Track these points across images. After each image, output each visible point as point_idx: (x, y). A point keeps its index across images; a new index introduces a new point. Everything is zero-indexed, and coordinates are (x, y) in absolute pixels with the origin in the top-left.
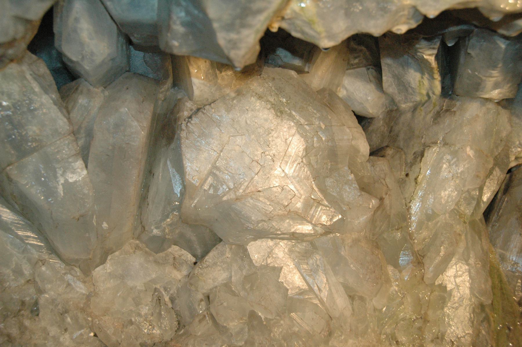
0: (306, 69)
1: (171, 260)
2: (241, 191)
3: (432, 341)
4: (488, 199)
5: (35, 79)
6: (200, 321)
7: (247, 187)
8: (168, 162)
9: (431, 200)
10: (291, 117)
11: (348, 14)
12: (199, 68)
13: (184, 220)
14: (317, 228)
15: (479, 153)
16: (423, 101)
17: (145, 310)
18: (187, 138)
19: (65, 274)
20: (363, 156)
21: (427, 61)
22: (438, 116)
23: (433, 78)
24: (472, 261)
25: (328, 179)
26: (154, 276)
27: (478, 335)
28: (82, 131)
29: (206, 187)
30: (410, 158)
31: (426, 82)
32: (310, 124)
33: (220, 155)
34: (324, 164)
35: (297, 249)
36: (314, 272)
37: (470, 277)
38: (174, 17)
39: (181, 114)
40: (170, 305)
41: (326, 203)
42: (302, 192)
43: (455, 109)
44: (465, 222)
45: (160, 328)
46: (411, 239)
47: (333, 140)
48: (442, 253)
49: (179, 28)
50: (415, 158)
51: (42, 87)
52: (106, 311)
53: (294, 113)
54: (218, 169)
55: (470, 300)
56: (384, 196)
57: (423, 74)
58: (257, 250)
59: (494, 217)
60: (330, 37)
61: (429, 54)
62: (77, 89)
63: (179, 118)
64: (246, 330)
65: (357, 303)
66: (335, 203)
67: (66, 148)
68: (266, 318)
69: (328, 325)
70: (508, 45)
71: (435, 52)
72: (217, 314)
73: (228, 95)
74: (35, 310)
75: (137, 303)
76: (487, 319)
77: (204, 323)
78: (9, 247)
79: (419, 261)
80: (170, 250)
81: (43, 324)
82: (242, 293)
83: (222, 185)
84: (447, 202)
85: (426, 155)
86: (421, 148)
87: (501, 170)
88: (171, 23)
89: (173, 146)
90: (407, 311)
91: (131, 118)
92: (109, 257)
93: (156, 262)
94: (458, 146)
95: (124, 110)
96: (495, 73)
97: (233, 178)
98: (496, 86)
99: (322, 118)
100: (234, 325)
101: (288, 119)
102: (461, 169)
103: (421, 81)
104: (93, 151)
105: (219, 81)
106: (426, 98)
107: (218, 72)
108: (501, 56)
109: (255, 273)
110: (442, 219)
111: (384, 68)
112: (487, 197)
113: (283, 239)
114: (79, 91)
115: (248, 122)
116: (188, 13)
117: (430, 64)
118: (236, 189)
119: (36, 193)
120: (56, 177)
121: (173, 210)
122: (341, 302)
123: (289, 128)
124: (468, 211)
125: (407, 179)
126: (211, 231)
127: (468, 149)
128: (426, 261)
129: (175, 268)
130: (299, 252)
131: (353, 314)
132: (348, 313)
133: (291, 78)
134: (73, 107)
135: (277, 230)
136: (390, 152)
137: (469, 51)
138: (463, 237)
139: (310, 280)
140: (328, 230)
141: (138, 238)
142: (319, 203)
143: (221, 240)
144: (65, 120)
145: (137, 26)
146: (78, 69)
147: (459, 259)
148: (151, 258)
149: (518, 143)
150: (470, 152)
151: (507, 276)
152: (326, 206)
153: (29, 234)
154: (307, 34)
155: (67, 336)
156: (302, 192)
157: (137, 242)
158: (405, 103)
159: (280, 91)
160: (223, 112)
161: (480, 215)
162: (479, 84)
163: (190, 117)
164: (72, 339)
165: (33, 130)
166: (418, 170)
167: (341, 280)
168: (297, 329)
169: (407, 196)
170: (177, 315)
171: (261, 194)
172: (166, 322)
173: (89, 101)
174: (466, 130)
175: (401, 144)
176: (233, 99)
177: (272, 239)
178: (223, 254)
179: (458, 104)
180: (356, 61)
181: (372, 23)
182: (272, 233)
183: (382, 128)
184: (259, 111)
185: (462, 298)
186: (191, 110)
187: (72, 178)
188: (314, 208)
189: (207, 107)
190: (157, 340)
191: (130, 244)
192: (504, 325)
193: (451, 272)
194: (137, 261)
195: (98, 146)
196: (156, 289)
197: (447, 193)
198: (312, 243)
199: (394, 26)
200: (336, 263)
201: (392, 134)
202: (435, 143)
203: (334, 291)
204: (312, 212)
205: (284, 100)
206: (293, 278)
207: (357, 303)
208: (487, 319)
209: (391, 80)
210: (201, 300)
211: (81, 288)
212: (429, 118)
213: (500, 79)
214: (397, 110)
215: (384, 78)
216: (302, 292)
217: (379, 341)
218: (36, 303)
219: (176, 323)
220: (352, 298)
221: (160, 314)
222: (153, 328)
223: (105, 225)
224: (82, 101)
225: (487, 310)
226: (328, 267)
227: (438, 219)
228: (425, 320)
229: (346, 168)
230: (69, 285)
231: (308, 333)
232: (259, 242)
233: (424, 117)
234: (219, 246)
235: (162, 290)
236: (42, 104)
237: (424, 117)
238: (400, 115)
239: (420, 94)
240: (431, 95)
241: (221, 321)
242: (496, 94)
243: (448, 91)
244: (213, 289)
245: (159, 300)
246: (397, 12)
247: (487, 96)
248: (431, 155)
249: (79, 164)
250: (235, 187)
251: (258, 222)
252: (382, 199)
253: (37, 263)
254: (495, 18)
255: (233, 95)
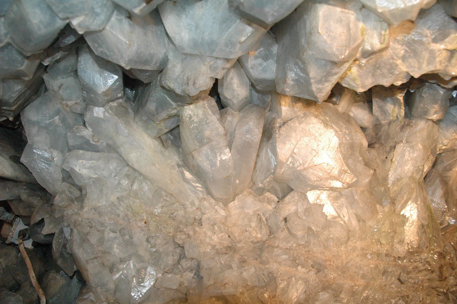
0: (338, 103)
1: (266, 200)
2: (307, 165)
3: (398, 243)
4: (427, 171)
5: (210, 108)
6: (282, 231)
7: (310, 163)
8: (269, 150)
9: (399, 170)
10: (332, 127)
11: (373, 76)
12: (285, 102)
13: (276, 180)
14: (344, 185)
15: (424, 147)
16: (394, 120)
17: (253, 225)
18: (279, 138)
19: (215, 205)
20: (365, 148)
21: (399, 99)
22: (403, 128)
23: (401, 108)
24: (419, 202)
25: (349, 160)
26: (258, 208)
27: (421, 240)
28: (228, 134)
29: (288, 163)
30: (388, 149)
31: (396, 110)
32: (341, 131)
33: (296, 146)
34: (348, 151)
35: (332, 195)
36: (340, 207)
37: (418, 211)
38: (289, 77)
39: (275, 125)
40: (266, 223)
41: (349, 172)
42: (337, 166)
43: (412, 124)
44: (416, 183)
45: (261, 234)
46: (389, 191)
47: (352, 139)
48: (405, 198)
49: (290, 82)
50: (391, 149)
51: (212, 112)
52: (234, 225)
53: (333, 125)
54: (295, 154)
55: (417, 222)
56: (376, 169)
57: (395, 105)
58: (312, 196)
59: (428, 180)
60: (363, 87)
61: (400, 97)
62: (226, 113)
63: (274, 127)
64: (306, 236)
65: (361, 223)
66: (354, 172)
67: (223, 142)
68: (316, 231)
69: (348, 234)
70: (444, 93)
71: (404, 95)
72: (291, 228)
73: (299, 115)
74: (200, 224)
75: (250, 221)
76: (425, 232)
77: (284, 232)
78: (189, 191)
79: (393, 202)
80: (266, 195)
81: (204, 230)
82: (304, 218)
83: (296, 162)
84: (408, 172)
85: (396, 147)
86: (394, 144)
87: (433, 156)
88: (287, 79)
89: (271, 141)
90: (386, 228)
91: (252, 128)
92: (237, 198)
93: (260, 201)
94: (414, 143)
95: (251, 123)
96: (436, 106)
97: (302, 158)
98: (435, 113)
99: (347, 128)
100: (300, 234)
101: (330, 128)
102: (415, 155)
103: (394, 109)
104: (234, 145)
105: (295, 109)
106: (396, 118)
107: (294, 104)
108: (440, 98)
109: (310, 207)
110: (405, 181)
111: (374, 102)
112: (426, 169)
113: (325, 190)
114: (227, 114)
115: (310, 130)
116: (296, 74)
117: (400, 101)
118: (304, 164)
119: (205, 165)
120: (216, 157)
121: (271, 174)
122: (354, 222)
123: (331, 133)
124: (418, 177)
125: (387, 160)
126: (288, 185)
127: (419, 145)
128: (397, 202)
129: (268, 204)
130: (333, 197)
131: (360, 229)
132: (357, 228)
133: (330, 107)
134: (225, 122)
135: (324, 185)
136: (377, 146)
137: (422, 95)
138: (415, 190)
139: (339, 211)
140: (349, 186)
141: (251, 188)
142: (346, 172)
143: (292, 190)
144: (223, 128)
145: (262, 81)
146: (229, 102)
147: (412, 202)
148: (257, 199)
149: (441, 142)
150: (420, 146)
151: (434, 210)
152: (349, 174)
153: (198, 185)
154: (351, 85)
155: (215, 236)
156: (337, 166)
157: (250, 190)
158: (384, 120)
159: (326, 114)
160: (297, 124)
161: (422, 179)
162: (427, 112)
163: (280, 127)
164: (218, 238)
165: (207, 133)
166: (392, 155)
167: (354, 212)
168: (332, 236)
169: (386, 169)
170: (269, 227)
171: (316, 167)
172: (264, 231)
173: (233, 118)
174: (418, 135)
175: (383, 142)
176: (302, 118)
177: (319, 190)
178: (293, 197)
179: (414, 121)
180: (359, 99)
181: (385, 80)
182: (321, 187)
183: (372, 133)
184: (316, 124)
185: (413, 222)
186: (280, 123)
187: (224, 157)
188: (343, 175)
189: (290, 122)
190: (259, 240)
191: (247, 191)
192: (433, 235)
193: (408, 208)
194: (250, 200)
195: (237, 142)
196: (258, 214)
197: (408, 167)
198: (340, 192)
199: (395, 82)
200: (352, 202)
201: (377, 136)
202: (402, 141)
203: (351, 217)
204: (342, 177)
205: (328, 119)
206: (329, 210)
207: (361, 223)
208: (425, 232)
209: (377, 109)
210: (282, 221)
211: (223, 213)
212: (398, 128)
213: (438, 109)
214: (380, 124)
215: (373, 108)
216: (335, 218)
217: (372, 243)
218: (201, 219)
219: (269, 232)
220: (359, 221)
221: (261, 227)
222: (257, 234)
223: (237, 181)
224: (229, 118)
225: (425, 227)
226: (348, 205)
227: (403, 181)
228: (395, 232)
229: (358, 154)
230: (216, 211)
231: (337, 238)
232: (312, 192)
233: (395, 128)
234: (292, 193)
235: (262, 214)
236: (212, 121)
237: (395, 128)
238: (382, 127)
239: (393, 116)
240: (399, 116)
241: (293, 231)
242: (435, 117)
243: (409, 115)
244: (289, 215)
245: (260, 220)
246: (398, 74)
247: (430, 118)
248: (399, 148)
249: (227, 150)
250: (303, 163)
251: (315, 181)
252: (375, 170)
253: (201, 200)
254: (447, 79)
255: (302, 115)
